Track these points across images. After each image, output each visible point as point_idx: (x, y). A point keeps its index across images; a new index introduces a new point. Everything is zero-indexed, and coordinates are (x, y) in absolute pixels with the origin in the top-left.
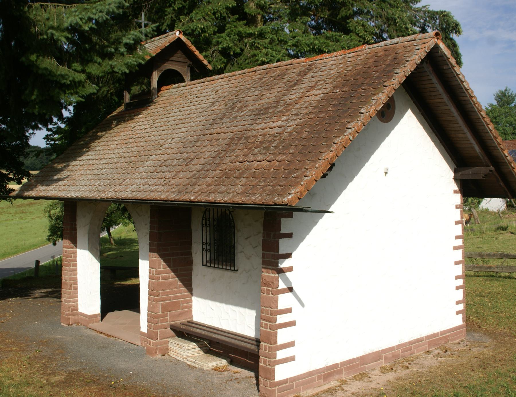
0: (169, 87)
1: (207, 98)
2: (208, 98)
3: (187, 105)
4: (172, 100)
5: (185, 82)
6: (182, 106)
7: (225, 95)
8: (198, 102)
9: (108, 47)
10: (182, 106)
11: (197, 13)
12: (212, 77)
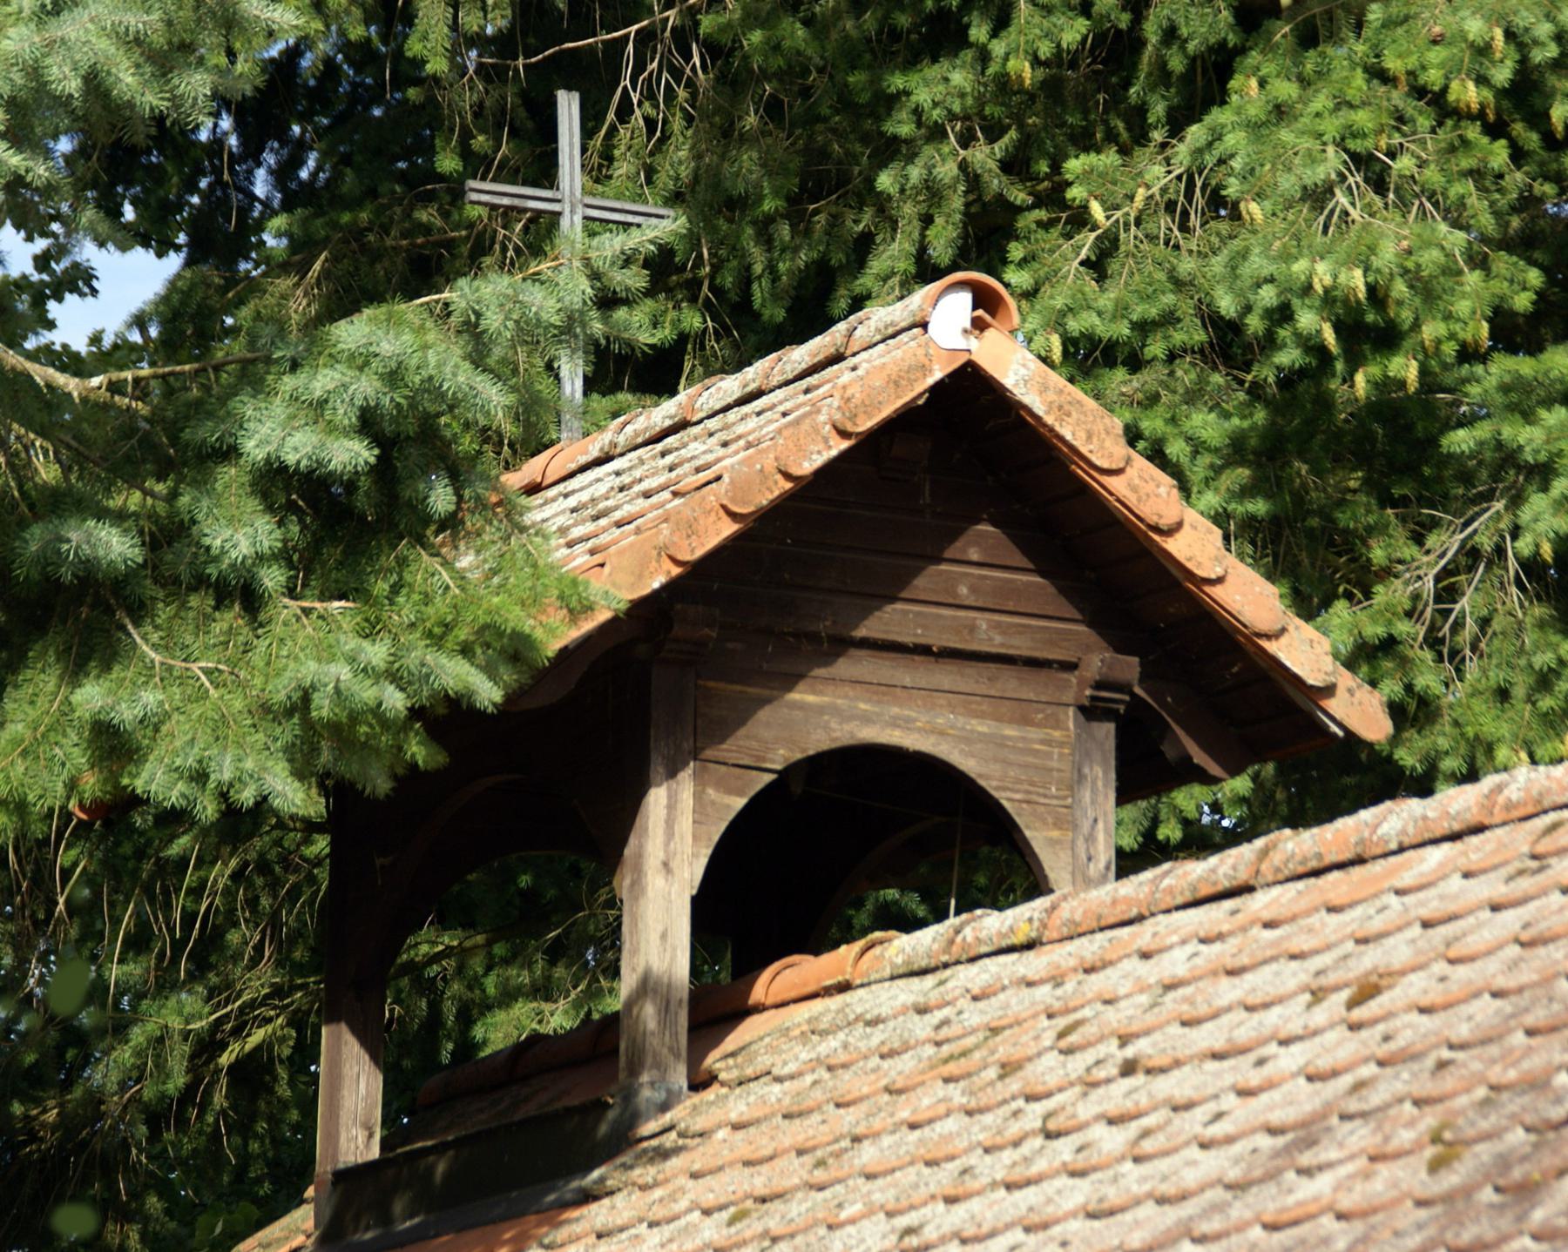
0: (840, 960)
1: (1241, 1071)
2: (1254, 1078)
3: (999, 1166)
4: (849, 1119)
5: (1034, 885)
6: (943, 1178)
7: (1463, 1031)
8: (1134, 1128)
9: (58, 504)
10: (943, 1178)
11: (1280, 112)
12: (1345, 824)
